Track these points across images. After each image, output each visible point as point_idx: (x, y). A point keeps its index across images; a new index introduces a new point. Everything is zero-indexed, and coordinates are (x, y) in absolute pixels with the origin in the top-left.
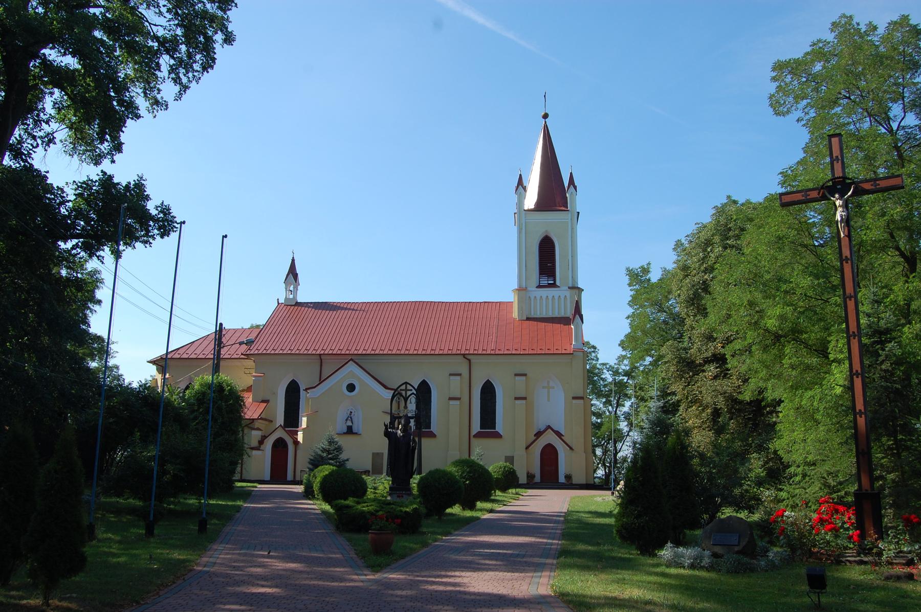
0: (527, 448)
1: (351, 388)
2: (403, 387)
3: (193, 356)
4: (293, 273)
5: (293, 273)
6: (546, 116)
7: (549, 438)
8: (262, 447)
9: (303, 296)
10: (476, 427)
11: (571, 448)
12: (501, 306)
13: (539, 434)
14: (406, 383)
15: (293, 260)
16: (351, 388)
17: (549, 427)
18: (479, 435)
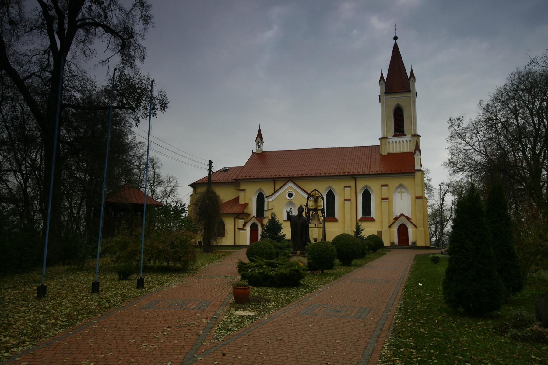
0: (390, 227)
1: (290, 195)
2: (314, 193)
3: (222, 181)
4: (260, 135)
5: (260, 135)
6: (396, 38)
7: (403, 220)
8: (245, 228)
9: (267, 147)
10: (360, 215)
11: (416, 226)
12: (349, 236)
13: (396, 219)
14: (315, 190)
15: (260, 129)
16: (290, 195)
17: (402, 215)
18: (362, 220)
